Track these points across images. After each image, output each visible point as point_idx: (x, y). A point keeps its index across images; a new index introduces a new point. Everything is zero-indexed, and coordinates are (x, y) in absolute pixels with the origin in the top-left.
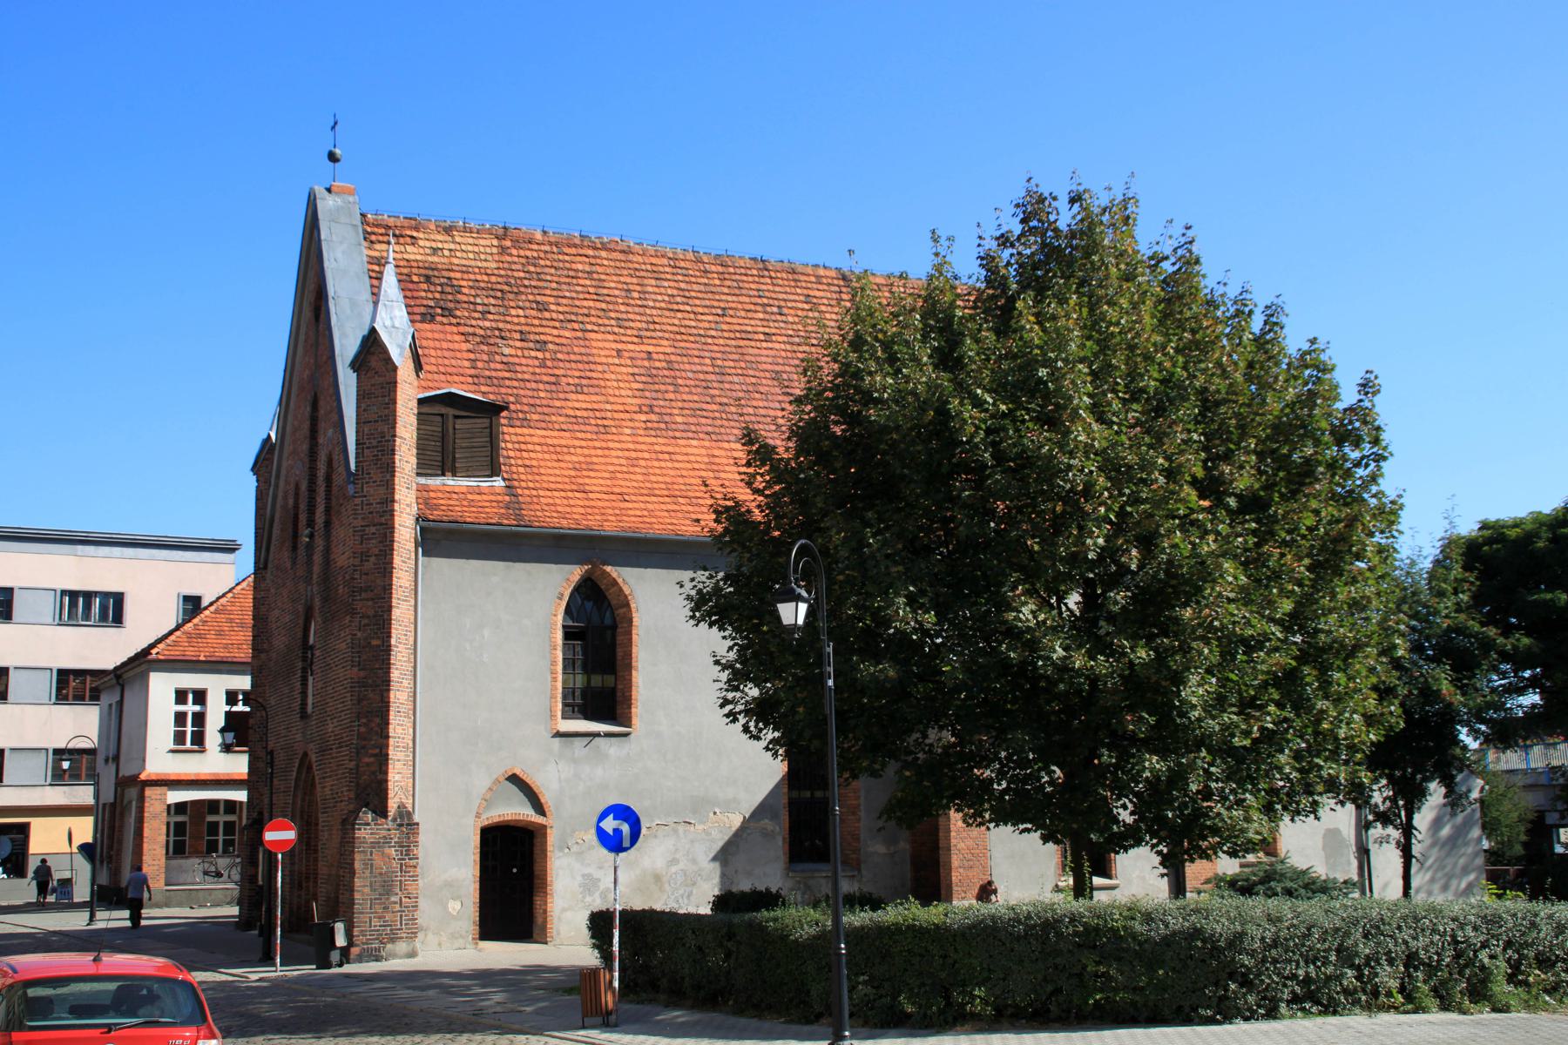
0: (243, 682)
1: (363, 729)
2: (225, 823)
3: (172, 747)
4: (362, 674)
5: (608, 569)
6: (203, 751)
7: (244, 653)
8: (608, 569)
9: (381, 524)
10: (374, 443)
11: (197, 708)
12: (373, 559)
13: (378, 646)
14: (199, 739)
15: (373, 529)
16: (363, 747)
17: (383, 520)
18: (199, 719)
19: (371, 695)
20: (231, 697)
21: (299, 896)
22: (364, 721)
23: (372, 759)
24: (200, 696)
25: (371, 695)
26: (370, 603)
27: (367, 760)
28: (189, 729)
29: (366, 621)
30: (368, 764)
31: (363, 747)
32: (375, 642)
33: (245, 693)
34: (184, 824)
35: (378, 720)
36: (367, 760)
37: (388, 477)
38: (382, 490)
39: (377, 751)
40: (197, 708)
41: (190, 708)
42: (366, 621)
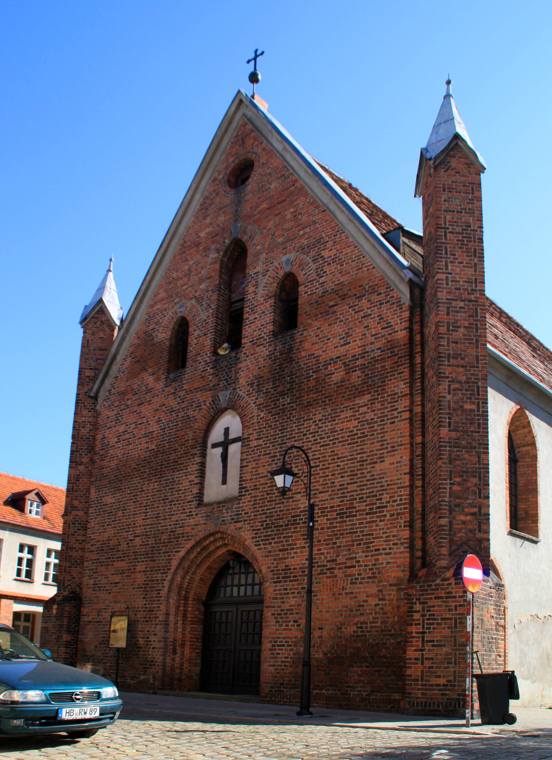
0: (57, 545)
1: (455, 488)
2: (24, 627)
3: (15, 577)
4: (454, 435)
5: (527, 413)
6: (32, 582)
7: (59, 530)
8: (527, 413)
9: (470, 301)
10: (458, 229)
11: (30, 556)
12: (462, 330)
13: (472, 410)
14: (29, 574)
15: (462, 304)
16: (458, 506)
17: (472, 297)
18: (30, 563)
19: (466, 456)
20: (49, 552)
21: (173, 660)
22: (458, 479)
23: (468, 518)
24: (32, 550)
25: (466, 456)
26: (461, 369)
27: (463, 518)
28: (24, 568)
29: (457, 386)
30: (464, 523)
31: (458, 506)
32: (468, 406)
33: (56, 551)
34: (28, 627)
35: (475, 481)
36: (463, 518)
37: (476, 260)
38: (470, 271)
39: (476, 510)
40: (30, 556)
41: (26, 555)
42: (457, 386)
